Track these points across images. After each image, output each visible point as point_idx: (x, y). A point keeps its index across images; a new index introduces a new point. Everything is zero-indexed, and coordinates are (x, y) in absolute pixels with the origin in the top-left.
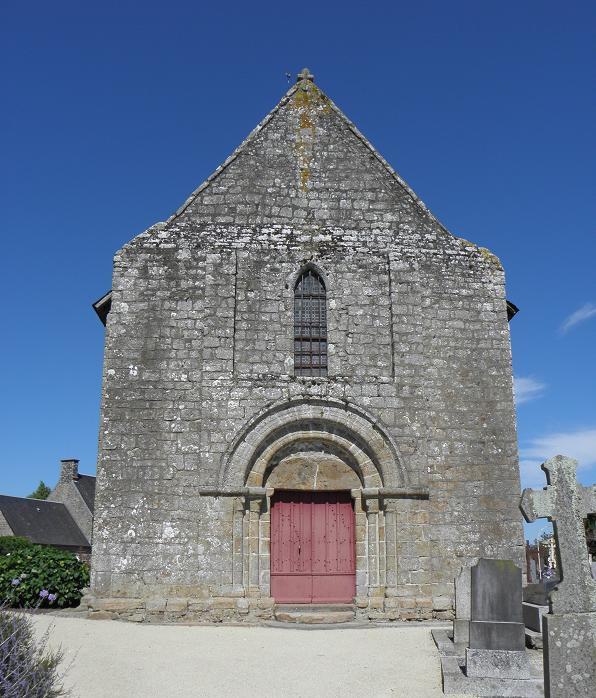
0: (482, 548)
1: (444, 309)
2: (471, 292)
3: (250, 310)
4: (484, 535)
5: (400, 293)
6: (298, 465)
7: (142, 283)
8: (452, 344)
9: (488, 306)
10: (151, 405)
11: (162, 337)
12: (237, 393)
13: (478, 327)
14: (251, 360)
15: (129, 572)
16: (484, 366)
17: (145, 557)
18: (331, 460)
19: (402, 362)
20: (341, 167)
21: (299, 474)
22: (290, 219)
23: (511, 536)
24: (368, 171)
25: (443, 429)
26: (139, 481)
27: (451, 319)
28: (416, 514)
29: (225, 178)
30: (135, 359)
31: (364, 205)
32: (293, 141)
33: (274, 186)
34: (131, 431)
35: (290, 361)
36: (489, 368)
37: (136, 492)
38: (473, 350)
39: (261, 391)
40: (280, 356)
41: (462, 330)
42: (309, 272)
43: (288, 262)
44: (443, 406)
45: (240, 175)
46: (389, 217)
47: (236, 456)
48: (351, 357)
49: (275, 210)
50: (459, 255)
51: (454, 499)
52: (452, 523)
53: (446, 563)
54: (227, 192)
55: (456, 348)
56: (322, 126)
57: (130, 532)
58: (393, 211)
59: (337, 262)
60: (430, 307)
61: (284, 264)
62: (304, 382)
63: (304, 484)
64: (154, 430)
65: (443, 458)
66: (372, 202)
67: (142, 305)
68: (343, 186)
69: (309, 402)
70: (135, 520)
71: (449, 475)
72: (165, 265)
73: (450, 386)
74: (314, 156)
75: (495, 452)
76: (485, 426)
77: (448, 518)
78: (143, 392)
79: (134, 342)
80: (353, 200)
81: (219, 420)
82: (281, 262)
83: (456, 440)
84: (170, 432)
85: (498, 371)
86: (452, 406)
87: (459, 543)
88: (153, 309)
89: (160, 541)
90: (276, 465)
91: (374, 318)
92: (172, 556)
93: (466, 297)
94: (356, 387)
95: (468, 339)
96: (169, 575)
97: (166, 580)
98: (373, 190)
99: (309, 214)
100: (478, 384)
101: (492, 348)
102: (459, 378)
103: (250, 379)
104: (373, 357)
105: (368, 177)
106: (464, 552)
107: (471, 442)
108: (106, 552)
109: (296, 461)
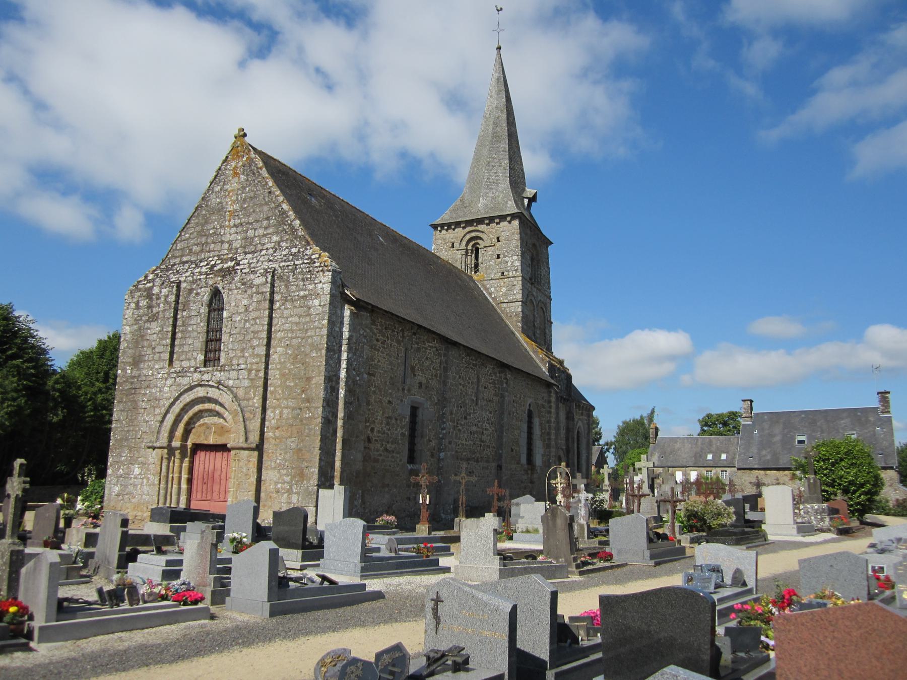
0: (291, 487)
1: (288, 308)
2: (307, 293)
3: (183, 325)
4: (293, 477)
5: (257, 302)
6: (203, 428)
7: (136, 312)
8: (290, 335)
9: (316, 302)
10: (135, 391)
11: (143, 347)
12: (169, 382)
13: (308, 319)
14: (181, 359)
15: (118, 495)
16: (308, 349)
17: (126, 486)
18: (220, 423)
19: (253, 353)
20: (251, 205)
21: (204, 433)
22: (219, 251)
23: (310, 479)
24: (267, 204)
25: (278, 400)
26: (127, 439)
27: (291, 316)
28: (250, 461)
29: (189, 228)
30: (130, 362)
31: (261, 232)
32: (227, 190)
33: (214, 228)
34: (125, 408)
35: (201, 357)
36: (311, 351)
37: (125, 446)
38: (302, 339)
39: (180, 380)
40: (195, 354)
41: (297, 324)
42: (216, 294)
43: (205, 287)
44: (279, 382)
45: (197, 223)
46: (275, 238)
47: (165, 423)
48: (230, 351)
49: (212, 246)
50: (303, 263)
51: (278, 452)
52: (275, 468)
53: (269, 497)
54: (189, 238)
55: (292, 338)
56: (243, 174)
57: (121, 470)
58: (277, 233)
59: (231, 283)
60: (279, 308)
61: (202, 289)
62: (200, 372)
63: (206, 440)
64: (136, 407)
65: (275, 421)
66: (266, 228)
67: (135, 326)
68: (251, 220)
69: (201, 386)
70: (123, 463)
71: (277, 433)
72: (147, 298)
73: (285, 368)
74: (237, 199)
75: (307, 416)
76: (303, 396)
77: (273, 464)
78: (132, 384)
79: (130, 351)
80: (255, 230)
81: (159, 400)
82: (201, 288)
83: (284, 407)
84: (141, 408)
85: (317, 353)
86: (285, 382)
87: (278, 483)
88: (140, 328)
89: (133, 476)
90: (194, 427)
91: (246, 321)
92: (136, 485)
93: (303, 297)
94: (226, 373)
95: (300, 330)
96: (134, 497)
97: (133, 500)
98: (268, 219)
99: (230, 246)
100: (303, 364)
101: (316, 335)
102: (291, 360)
103: (175, 372)
104: (243, 350)
105: (266, 208)
106: (280, 489)
107: (294, 409)
108: (110, 483)
109: (203, 424)
